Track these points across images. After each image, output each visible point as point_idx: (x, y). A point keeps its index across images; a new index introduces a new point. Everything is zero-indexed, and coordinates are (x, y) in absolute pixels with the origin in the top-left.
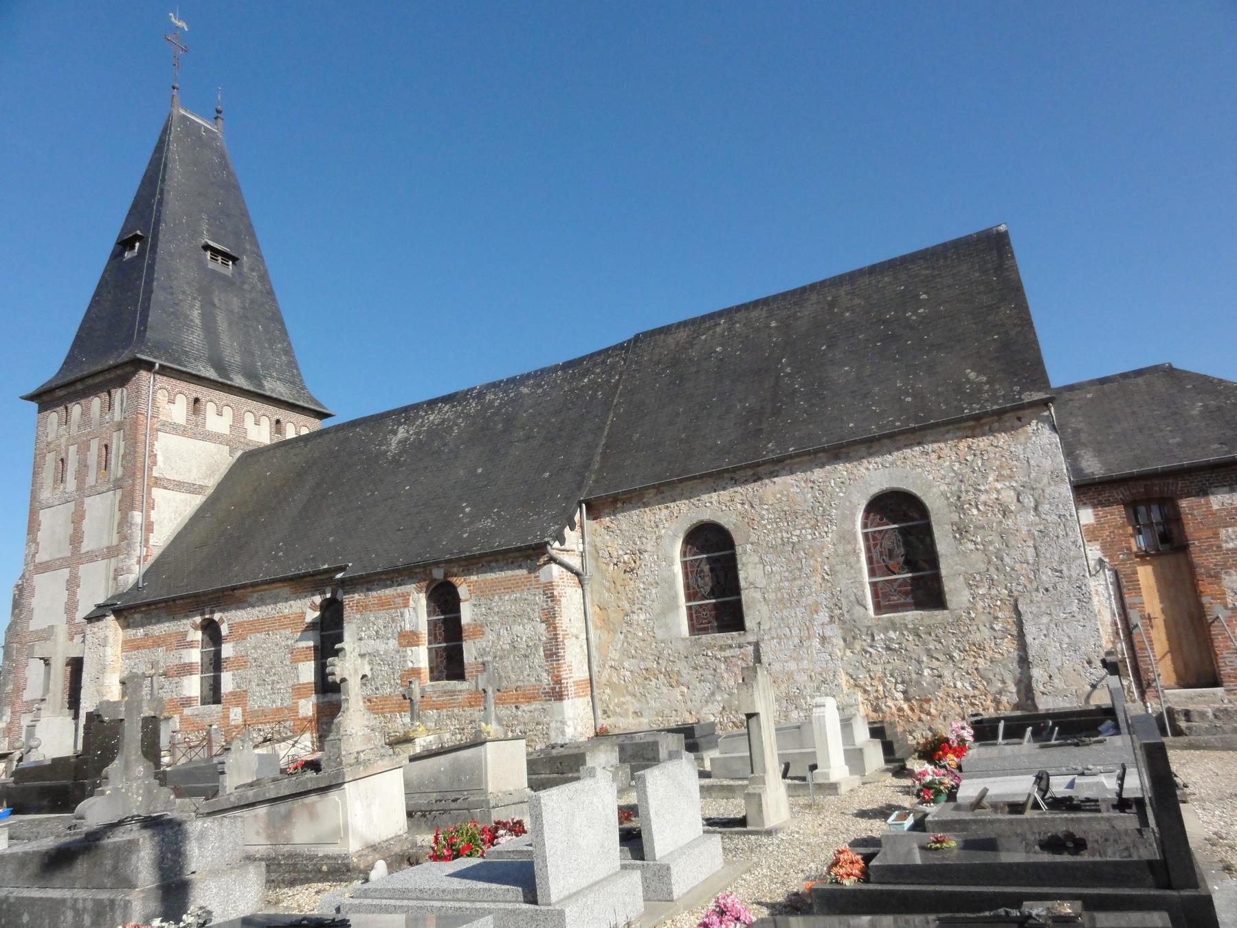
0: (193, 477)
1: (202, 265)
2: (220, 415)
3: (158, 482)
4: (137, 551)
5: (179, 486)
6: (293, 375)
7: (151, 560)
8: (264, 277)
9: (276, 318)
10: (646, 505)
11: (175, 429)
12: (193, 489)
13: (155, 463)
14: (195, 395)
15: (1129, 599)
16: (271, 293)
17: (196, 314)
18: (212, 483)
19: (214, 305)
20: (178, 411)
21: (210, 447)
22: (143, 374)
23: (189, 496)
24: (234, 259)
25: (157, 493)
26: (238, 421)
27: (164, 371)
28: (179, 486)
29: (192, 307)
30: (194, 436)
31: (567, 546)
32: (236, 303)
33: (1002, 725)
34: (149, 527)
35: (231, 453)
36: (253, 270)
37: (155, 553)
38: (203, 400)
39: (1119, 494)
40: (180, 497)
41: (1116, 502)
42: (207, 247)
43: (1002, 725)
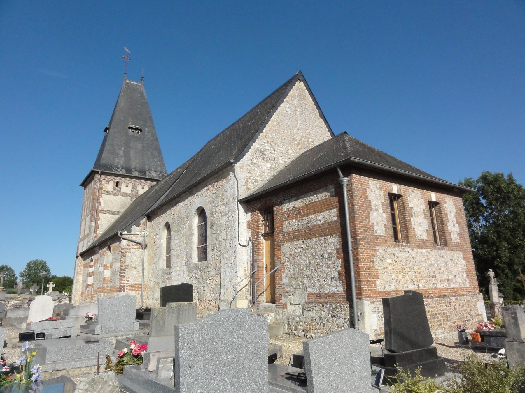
0: (116, 209)
1: (127, 134)
2: (127, 187)
3: (101, 212)
4: (93, 235)
5: (110, 212)
6: (162, 169)
7: (97, 238)
8: (154, 135)
9: (158, 149)
10: (158, 216)
11: (109, 193)
12: (118, 213)
13: (100, 205)
14: (117, 180)
15: (256, 258)
16: (157, 139)
17: (122, 152)
18: (123, 210)
19: (130, 148)
20: (110, 186)
21: (123, 198)
22: (97, 175)
23: (113, 216)
24: (141, 130)
25: (101, 215)
26: (135, 188)
27: (103, 173)
28: (110, 212)
29: (121, 150)
30: (116, 195)
31: (132, 233)
32: (140, 146)
33: (20, 286)
34: (97, 227)
35: (132, 199)
36: (149, 132)
37: (99, 235)
38: (120, 182)
39: (258, 205)
40: (109, 216)
41: (257, 210)
42: (130, 128)
43: (20, 286)
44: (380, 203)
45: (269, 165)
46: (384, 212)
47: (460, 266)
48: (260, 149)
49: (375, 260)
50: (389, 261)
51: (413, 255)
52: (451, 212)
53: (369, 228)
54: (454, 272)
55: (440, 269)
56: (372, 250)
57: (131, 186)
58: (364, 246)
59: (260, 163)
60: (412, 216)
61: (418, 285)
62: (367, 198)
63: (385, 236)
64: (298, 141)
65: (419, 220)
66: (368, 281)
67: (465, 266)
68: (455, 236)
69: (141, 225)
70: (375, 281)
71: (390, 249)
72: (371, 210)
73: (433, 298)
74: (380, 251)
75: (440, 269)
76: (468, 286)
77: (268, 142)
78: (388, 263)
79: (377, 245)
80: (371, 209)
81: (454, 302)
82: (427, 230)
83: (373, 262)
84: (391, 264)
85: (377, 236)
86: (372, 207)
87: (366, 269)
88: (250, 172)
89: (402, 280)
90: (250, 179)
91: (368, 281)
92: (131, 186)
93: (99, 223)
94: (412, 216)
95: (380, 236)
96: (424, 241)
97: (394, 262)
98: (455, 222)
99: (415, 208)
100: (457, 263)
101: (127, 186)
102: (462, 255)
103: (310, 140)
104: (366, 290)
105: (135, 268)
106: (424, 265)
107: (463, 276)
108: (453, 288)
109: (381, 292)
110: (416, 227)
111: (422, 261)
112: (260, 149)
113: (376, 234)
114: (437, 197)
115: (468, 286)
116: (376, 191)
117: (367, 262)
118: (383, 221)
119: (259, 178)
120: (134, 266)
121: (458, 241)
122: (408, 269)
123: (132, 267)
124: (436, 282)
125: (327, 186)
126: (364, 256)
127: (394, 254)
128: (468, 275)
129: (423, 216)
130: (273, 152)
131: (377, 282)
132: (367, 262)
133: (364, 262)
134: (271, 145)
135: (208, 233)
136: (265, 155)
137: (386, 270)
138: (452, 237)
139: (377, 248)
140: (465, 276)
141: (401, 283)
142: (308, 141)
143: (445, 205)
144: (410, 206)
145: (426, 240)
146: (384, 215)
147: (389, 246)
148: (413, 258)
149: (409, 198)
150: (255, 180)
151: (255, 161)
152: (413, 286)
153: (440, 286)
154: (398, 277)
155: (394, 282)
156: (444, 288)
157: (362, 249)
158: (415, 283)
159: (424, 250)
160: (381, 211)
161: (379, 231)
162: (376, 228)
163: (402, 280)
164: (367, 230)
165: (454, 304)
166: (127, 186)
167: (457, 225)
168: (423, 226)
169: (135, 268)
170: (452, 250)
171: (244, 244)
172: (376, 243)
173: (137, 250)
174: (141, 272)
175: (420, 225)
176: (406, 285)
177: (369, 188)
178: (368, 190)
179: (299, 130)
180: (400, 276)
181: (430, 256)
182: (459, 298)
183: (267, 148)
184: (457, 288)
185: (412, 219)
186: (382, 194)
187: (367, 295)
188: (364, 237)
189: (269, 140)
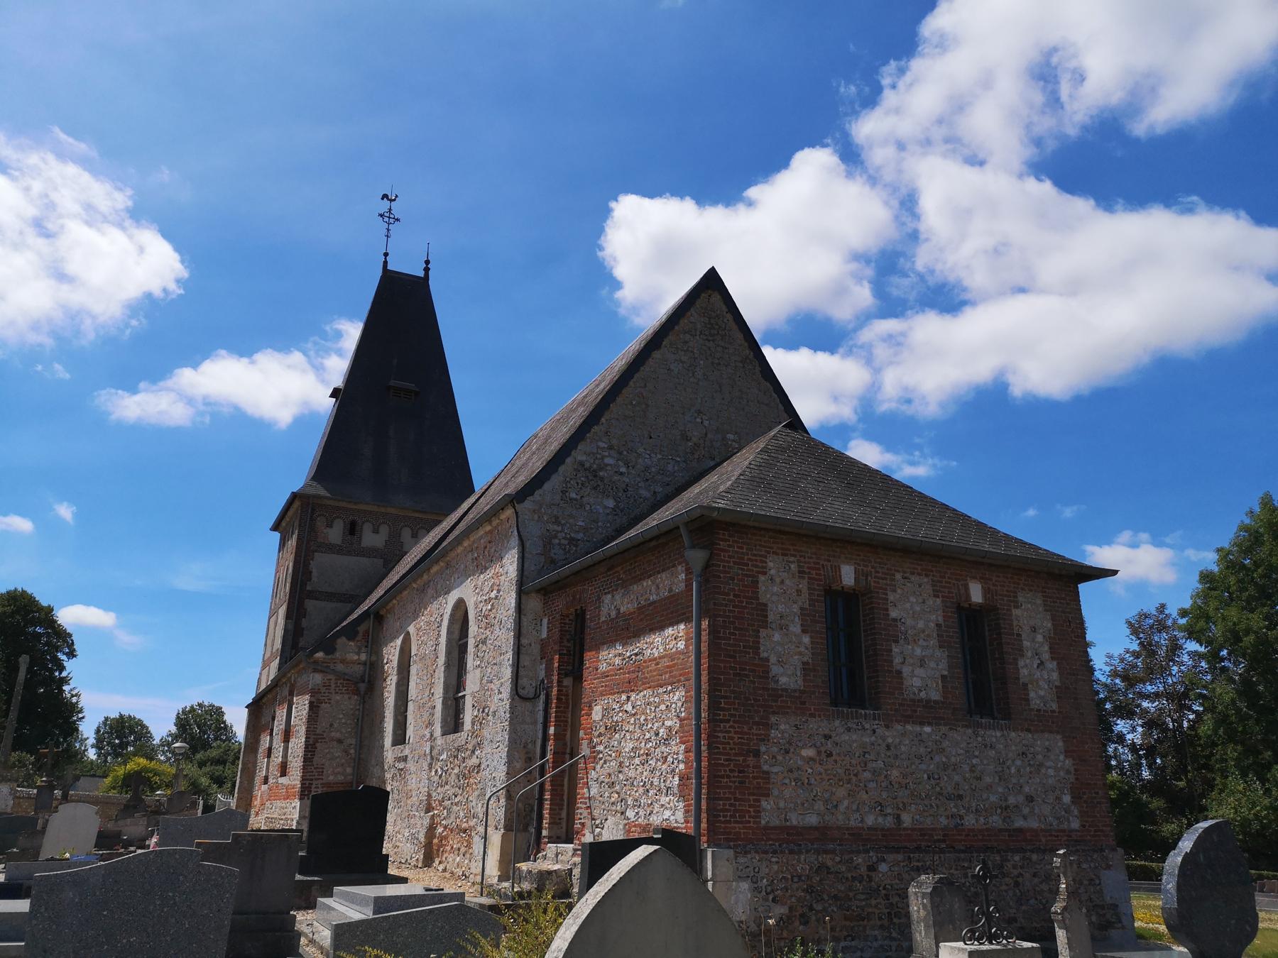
5: (330, 597)
11: (331, 548)
21: (365, 561)
30: (349, 553)
44: (796, 609)
45: (611, 503)
46: (804, 631)
47: (1051, 772)
48: (587, 465)
49: (763, 749)
50: (808, 752)
51: (890, 740)
52: (1034, 629)
53: (754, 671)
54: (1027, 789)
55: (979, 779)
56: (757, 724)
57: (384, 530)
58: (731, 715)
59: (585, 500)
60: (896, 642)
61: (898, 817)
62: (758, 599)
63: (802, 692)
64: (694, 439)
65: (918, 651)
66: (736, 799)
67: (1068, 772)
68: (1042, 693)
69: (360, 637)
70: (759, 801)
71: (813, 725)
72: (766, 627)
73: (942, 851)
74: (783, 728)
75: (979, 779)
76: (1075, 825)
77: (611, 448)
78: (802, 758)
79: (774, 713)
80: (764, 623)
81: (1014, 867)
82: (943, 677)
83: (757, 754)
84: (811, 759)
85: (774, 689)
86: (771, 617)
87: (731, 771)
88: (556, 521)
89: (846, 803)
90: (556, 537)
91: (736, 799)
92: (384, 530)
93: (304, 623)
94: (896, 642)
95: (786, 690)
96: (928, 704)
97: (824, 755)
98: (1046, 656)
99: (909, 622)
100: (1041, 765)
101: (376, 531)
102: (1060, 744)
103: (730, 436)
104: (729, 822)
105: (340, 741)
106: (923, 767)
107: (1058, 798)
108: (1020, 830)
109: (775, 828)
110: (906, 670)
111: (920, 757)
112: (587, 465)
113: (772, 685)
114: (986, 592)
115: (1075, 825)
116: (787, 582)
117: (736, 755)
118: (800, 653)
119: (580, 536)
120: (338, 735)
121: (1054, 706)
122: (867, 775)
123: (332, 740)
124: (963, 812)
125: (674, 566)
126: (732, 738)
127: (827, 737)
128: (1076, 799)
129: (933, 642)
130: (623, 470)
131: (764, 804)
132: (736, 755)
133: (728, 754)
134: (621, 453)
135: (471, 662)
136: (602, 479)
137: (795, 775)
138: (1032, 695)
139: (773, 719)
140: (1067, 799)
141: (842, 808)
142: (724, 439)
143: (1016, 612)
144: (894, 614)
145: (935, 702)
146: (806, 639)
147: (812, 715)
148: (888, 747)
149: (891, 597)
150: (572, 539)
151: (573, 495)
152: (880, 820)
153: (970, 821)
154: (833, 794)
155: (819, 806)
156: (987, 830)
157: (728, 721)
158: (889, 811)
159: (927, 729)
160: (796, 628)
161: (783, 680)
162: (775, 669)
163: (846, 803)
164: (746, 676)
165: (1016, 872)
166: (376, 531)
167: (1052, 665)
168: (932, 665)
169: (340, 741)
170: (1028, 730)
171: (531, 695)
172: (771, 707)
173: (346, 696)
174: (352, 751)
175: (922, 663)
176: (857, 815)
177: (765, 573)
178: (762, 578)
179: (699, 412)
180: (841, 792)
181: (946, 743)
182: (1034, 857)
183: (607, 461)
184: (1032, 830)
185: (895, 650)
186: (804, 586)
187: (730, 833)
188: (734, 692)
189: (614, 442)
